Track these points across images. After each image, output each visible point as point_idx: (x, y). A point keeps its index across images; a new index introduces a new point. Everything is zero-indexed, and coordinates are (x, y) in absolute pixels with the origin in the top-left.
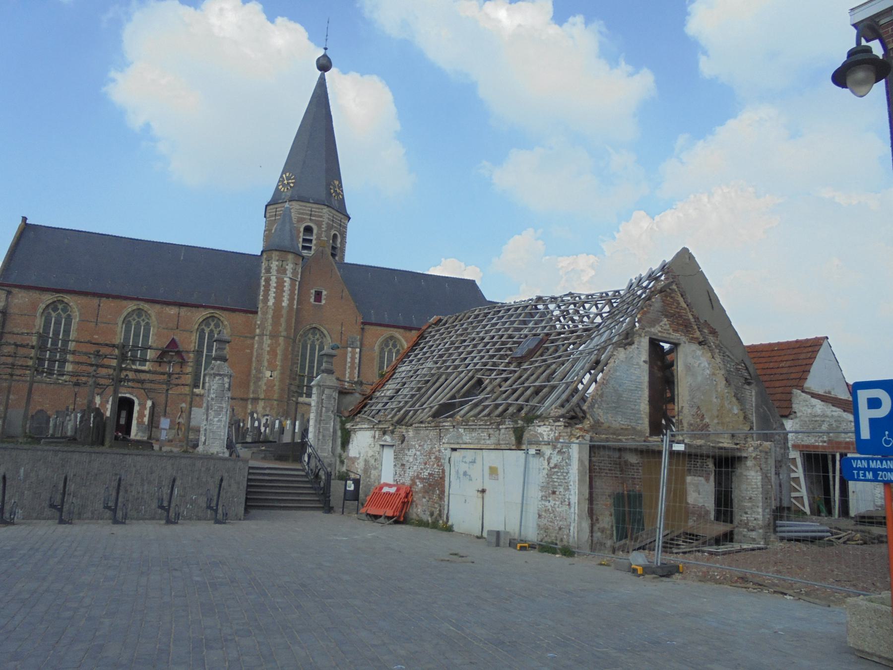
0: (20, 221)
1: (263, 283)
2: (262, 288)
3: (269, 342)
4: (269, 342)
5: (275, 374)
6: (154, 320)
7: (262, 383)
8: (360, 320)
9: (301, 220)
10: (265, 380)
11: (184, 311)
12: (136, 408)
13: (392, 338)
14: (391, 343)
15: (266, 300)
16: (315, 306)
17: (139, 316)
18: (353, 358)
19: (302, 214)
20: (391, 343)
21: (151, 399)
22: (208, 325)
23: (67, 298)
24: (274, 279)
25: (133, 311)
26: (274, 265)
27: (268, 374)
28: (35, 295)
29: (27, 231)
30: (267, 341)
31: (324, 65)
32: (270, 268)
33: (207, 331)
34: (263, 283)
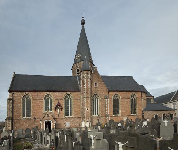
1: (82, 82)
2: (82, 83)
4: (86, 99)
5: (88, 109)
6: (52, 98)
7: (85, 112)
8: (107, 90)
11: (60, 93)
12: (52, 124)
13: (116, 95)
14: (116, 96)
15: (83, 86)
17: (48, 96)
18: (107, 101)
20: (116, 96)
21: (55, 120)
22: (67, 97)
24: (85, 79)
25: (47, 95)
26: (85, 75)
27: (87, 109)
28: (20, 93)
29: (16, 77)
30: (85, 99)
31: (83, 23)
33: (67, 99)
34: (82, 82)
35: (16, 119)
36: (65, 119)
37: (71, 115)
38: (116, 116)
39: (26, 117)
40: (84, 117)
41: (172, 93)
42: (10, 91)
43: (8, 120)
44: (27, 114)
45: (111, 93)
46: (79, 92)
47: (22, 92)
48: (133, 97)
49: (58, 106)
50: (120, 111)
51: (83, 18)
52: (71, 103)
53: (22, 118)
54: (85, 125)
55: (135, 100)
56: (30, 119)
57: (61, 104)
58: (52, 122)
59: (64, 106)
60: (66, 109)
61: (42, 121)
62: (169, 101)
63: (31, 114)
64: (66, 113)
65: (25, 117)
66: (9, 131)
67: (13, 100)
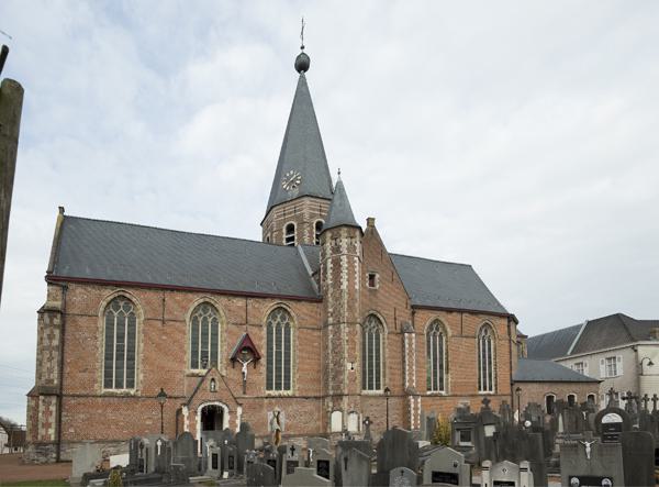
0: (57, 213)
1: (330, 265)
2: (330, 271)
3: (347, 330)
4: (347, 330)
5: (355, 366)
7: (345, 377)
9: (312, 216)
10: (347, 372)
11: (251, 301)
13: (436, 321)
14: (435, 326)
16: (370, 291)
19: (314, 209)
21: (241, 405)
23: (130, 293)
24: (344, 258)
28: (93, 291)
31: (302, 66)
32: (339, 247)
33: (274, 325)
34: (330, 265)
35: (73, 396)
36: (266, 401)
37: (287, 387)
38: (436, 395)
39: (116, 387)
40: (339, 397)
41: (569, 329)
42: (51, 279)
43: (42, 397)
44: (120, 376)
45: (420, 314)
46: (316, 302)
47: (104, 284)
48: (483, 334)
49: (245, 348)
50: (447, 379)
51: (302, 48)
52: (288, 340)
53: (99, 393)
54: (343, 426)
55: (489, 342)
56: (134, 396)
57: (256, 342)
58: (226, 410)
59: (263, 352)
60: (269, 362)
61: (187, 404)
62: (565, 354)
63: (139, 377)
64: (269, 379)
65: (111, 387)
66: (46, 445)
67: (62, 313)
